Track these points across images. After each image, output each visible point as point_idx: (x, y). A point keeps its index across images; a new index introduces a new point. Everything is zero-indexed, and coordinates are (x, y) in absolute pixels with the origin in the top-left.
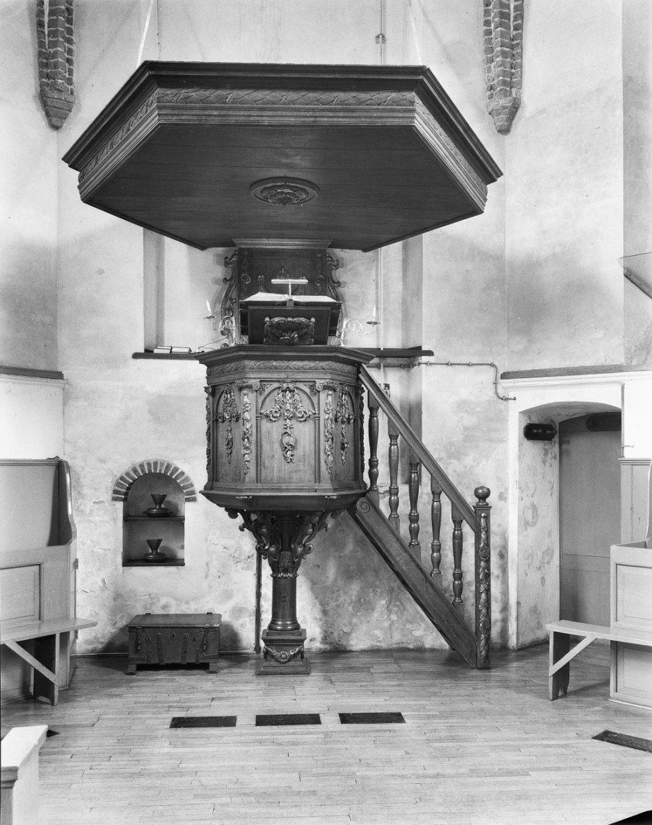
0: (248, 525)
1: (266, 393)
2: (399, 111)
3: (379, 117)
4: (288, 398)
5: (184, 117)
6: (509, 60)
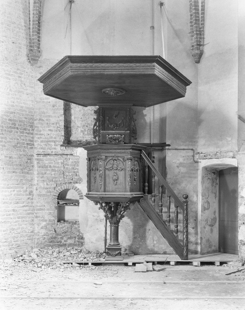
0: (101, 207)
1: (107, 161)
2: (150, 69)
3: (143, 71)
4: (115, 162)
5: (79, 72)
6: (199, 36)
